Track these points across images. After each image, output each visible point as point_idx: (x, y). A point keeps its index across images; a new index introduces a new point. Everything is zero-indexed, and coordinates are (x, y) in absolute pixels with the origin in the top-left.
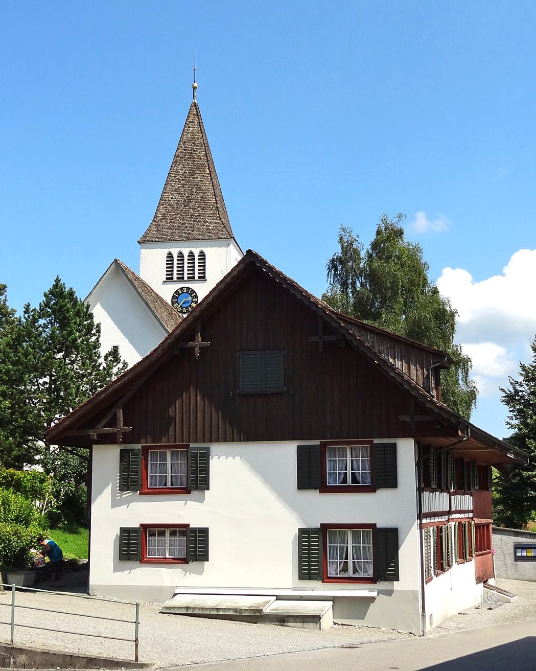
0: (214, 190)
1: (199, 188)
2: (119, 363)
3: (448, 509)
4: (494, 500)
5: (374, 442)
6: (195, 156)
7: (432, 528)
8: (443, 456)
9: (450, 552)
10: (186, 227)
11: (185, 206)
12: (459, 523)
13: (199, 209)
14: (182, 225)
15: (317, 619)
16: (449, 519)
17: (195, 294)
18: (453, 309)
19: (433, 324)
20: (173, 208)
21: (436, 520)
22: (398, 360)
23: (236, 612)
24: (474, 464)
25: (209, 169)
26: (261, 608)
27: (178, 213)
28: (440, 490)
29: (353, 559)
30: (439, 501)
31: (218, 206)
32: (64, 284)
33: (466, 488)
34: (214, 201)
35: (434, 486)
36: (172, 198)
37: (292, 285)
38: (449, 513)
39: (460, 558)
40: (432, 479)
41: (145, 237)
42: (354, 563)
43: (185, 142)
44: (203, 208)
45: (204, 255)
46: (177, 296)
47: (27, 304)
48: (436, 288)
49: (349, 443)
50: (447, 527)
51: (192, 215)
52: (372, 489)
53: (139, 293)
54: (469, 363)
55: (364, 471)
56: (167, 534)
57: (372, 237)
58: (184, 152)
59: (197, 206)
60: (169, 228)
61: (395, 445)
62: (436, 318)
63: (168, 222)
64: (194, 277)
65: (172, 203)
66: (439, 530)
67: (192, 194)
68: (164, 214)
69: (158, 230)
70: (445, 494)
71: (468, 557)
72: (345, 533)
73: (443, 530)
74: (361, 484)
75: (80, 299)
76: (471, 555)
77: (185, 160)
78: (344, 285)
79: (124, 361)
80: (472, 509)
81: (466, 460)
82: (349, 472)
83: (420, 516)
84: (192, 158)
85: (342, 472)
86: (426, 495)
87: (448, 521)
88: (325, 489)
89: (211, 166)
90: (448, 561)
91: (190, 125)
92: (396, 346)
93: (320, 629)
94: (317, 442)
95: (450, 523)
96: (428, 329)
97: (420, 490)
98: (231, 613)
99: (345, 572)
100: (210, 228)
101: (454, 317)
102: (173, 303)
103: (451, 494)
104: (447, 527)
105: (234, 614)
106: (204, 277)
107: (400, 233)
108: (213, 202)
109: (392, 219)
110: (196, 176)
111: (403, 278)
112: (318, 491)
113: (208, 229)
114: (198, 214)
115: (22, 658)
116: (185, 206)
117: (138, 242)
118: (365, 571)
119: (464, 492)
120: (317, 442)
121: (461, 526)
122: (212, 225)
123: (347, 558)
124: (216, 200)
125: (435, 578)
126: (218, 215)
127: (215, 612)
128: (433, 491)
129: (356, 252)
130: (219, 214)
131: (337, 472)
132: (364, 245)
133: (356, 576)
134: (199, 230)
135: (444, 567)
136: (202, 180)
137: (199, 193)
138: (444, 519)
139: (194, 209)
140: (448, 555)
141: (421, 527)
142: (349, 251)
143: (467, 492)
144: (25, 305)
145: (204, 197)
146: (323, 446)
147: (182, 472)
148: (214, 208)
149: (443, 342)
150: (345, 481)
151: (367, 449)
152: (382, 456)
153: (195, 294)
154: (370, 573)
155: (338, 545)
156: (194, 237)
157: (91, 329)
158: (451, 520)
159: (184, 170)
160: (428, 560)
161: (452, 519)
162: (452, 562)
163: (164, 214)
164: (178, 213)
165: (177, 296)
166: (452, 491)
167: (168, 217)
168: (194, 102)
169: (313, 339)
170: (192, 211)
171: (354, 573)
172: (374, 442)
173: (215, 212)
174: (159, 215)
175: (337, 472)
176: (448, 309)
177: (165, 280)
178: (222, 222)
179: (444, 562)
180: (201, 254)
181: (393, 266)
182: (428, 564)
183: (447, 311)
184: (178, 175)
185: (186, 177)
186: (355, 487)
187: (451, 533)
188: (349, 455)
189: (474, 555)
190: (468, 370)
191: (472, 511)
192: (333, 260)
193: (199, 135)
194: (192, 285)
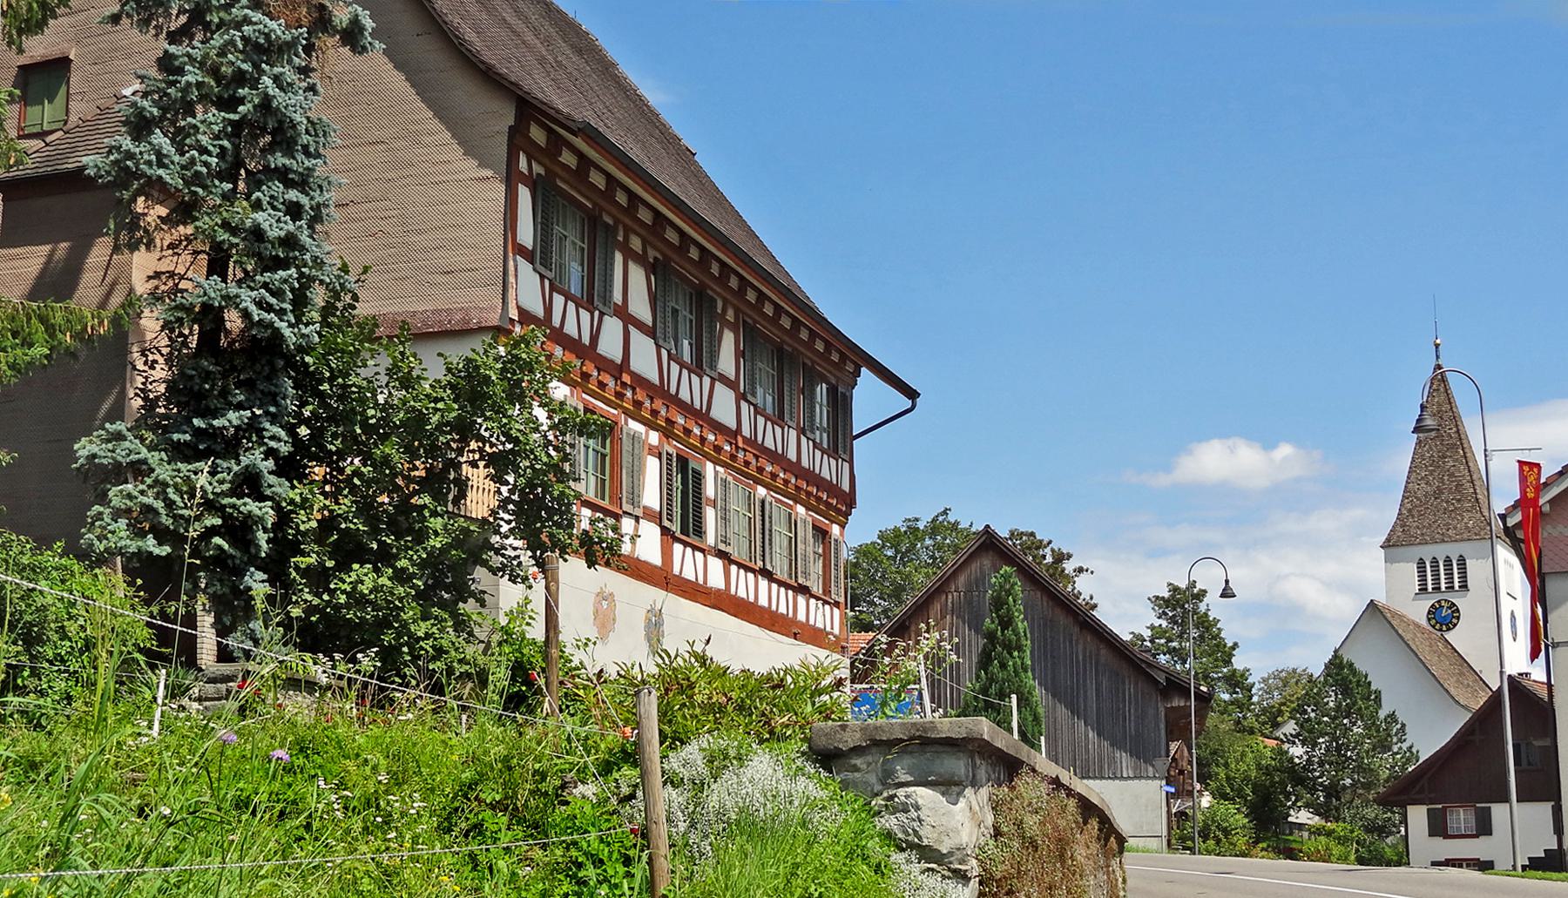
4: (1258, 829)
22: (970, 630)
25: (1463, 450)
31: (1479, 496)
34: (1472, 490)
41: (1388, 540)
44: (1459, 501)
60: (1418, 528)
68: (1410, 511)
88: (1447, 836)
89: (1465, 446)
106: (1466, 586)
113: (1467, 528)
134: (1455, 528)
137: (1453, 482)
139: (1447, 502)
156: (1450, 537)
163: (1410, 511)
167: (1415, 513)
193: (1446, 407)
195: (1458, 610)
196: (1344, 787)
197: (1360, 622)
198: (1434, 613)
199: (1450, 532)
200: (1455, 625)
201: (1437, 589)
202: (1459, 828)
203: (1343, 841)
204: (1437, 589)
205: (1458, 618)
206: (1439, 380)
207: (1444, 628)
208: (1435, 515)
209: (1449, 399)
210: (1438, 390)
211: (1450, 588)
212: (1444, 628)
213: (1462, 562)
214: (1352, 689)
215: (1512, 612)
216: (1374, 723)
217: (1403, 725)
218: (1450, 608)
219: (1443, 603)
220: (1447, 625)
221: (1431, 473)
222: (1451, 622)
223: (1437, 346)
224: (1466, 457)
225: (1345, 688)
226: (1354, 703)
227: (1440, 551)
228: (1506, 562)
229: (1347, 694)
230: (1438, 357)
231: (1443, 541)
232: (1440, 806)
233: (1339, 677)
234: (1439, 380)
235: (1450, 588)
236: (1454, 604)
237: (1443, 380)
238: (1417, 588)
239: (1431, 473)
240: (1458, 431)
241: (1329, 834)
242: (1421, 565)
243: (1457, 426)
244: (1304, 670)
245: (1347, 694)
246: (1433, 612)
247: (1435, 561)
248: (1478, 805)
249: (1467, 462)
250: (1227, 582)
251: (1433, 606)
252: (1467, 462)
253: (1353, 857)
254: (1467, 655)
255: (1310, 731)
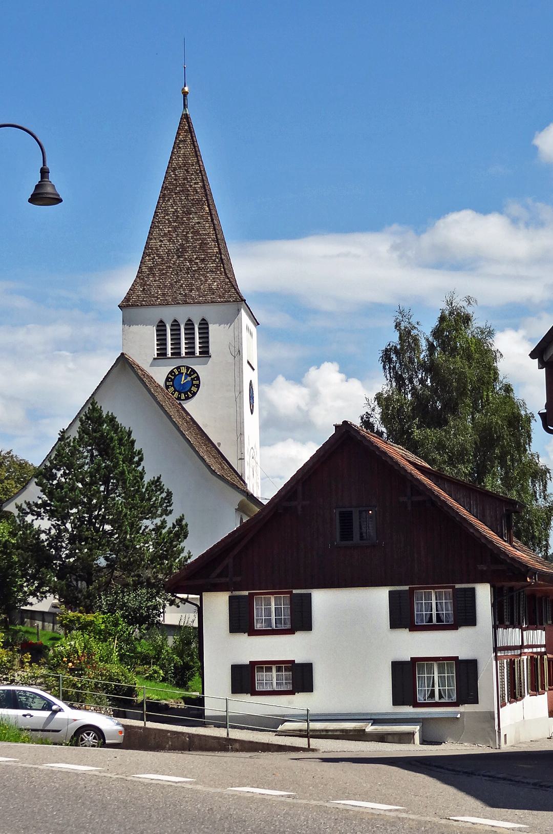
0: (216, 236)
1: (196, 233)
2: (162, 492)
3: (521, 644)
5: (456, 587)
6: (189, 188)
7: (505, 661)
8: (515, 598)
9: (523, 684)
10: (181, 286)
11: (179, 257)
12: (531, 657)
13: (197, 261)
14: (176, 282)
15: (412, 736)
16: (521, 653)
17: (196, 375)
18: (528, 412)
19: (506, 432)
20: (163, 259)
21: (510, 653)
23: (343, 732)
24: (546, 599)
25: (209, 206)
26: (364, 728)
27: (170, 267)
28: (513, 626)
29: (439, 687)
30: (512, 636)
32: (101, 407)
33: (538, 623)
34: (216, 250)
35: (507, 623)
36: (161, 246)
37: (493, 605)
38: (522, 647)
39: (532, 691)
40: (505, 617)
41: (127, 299)
42: (439, 690)
43: (175, 169)
45: (207, 324)
46: (173, 377)
47: (62, 430)
48: (509, 386)
49: (434, 588)
50: (520, 660)
51: (188, 269)
52: (454, 627)
53: (158, 403)
54: (548, 474)
55: (448, 610)
56: (274, 670)
57: (435, 323)
58: (175, 182)
59: (195, 257)
61: (473, 590)
62: (510, 424)
63: (157, 279)
64: (194, 352)
65: (162, 253)
66: (511, 664)
67: (188, 242)
68: (151, 269)
69: (144, 289)
70: (517, 629)
71: (540, 690)
72: (432, 665)
73: (516, 662)
74: (445, 623)
75: (121, 424)
76: (543, 688)
77: (176, 193)
78: (399, 379)
79: (168, 490)
80: (544, 643)
81: (538, 595)
82: (434, 612)
83: (496, 649)
84: (185, 191)
85: (429, 613)
86: (500, 630)
87: (520, 655)
90: (521, 692)
91: (181, 146)
92: (471, 494)
93: (414, 743)
94: (406, 588)
95: (522, 657)
96: (500, 438)
97: (495, 628)
98: (338, 733)
99: (432, 698)
100: (213, 287)
101: (530, 422)
102: (167, 387)
103: (523, 630)
104: (520, 660)
105: (341, 734)
106: (207, 352)
107: (467, 319)
108: (215, 251)
109: (459, 302)
110: (191, 216)
111: (472, 373)
112: (246, 634)
113: (210, 289)
114: (196, 268)
115: (237, 746)
116: (179, 257)
117: (119, 306)
118: (450, 697)
119: (536, 627)
120: (406, 588)
121: (533, 661)
122: (216, 284)
123: (433, 686)
124: (220, 250)
125: (508, 704)
126: (222, 270)
127: (324, 733)
128: (506, 627)
129: (416, 340)
130: (224, 268)
131: (424, 613)
132: (425, 329)
133: (442, 701)
134: (198, 289)
135: (517, 696)
136: (200, 221)
137: (197, 240)
138: (518, 652)
139: (191, 261)
140: (521, 687)
141: (496, 658)
142: (407, 336)
143: (539, 627)
144: (60, 431)
145: (203, 244)
146: (411, 591)
147: (286, 616)
148: (217, 260)
149: (519, 451)
150: (431, 620)
151: (449, 594)
152: (463, 599)
153: (196, 375)
154: (454, 698)
155: (426, 675)
156: (193, 299)
157: (133, 457)
158: (523, 654)
159: (175, 208)
160: (503, 688)
161: (525, 653)
162: (524, 693)
163: (151, 269)
164: (170, 267)
165: (173, 377)
166: (524, 626)
168: (184, 113)
169: (401, 499)
170: (188, 264)
171: (440, 699)
172: (456, 587)
173: (219, 265)
174: (145, 269)
175: (424, 613)
176: (523, 413)
177: (156, 356)
178: (228, 278)
179: (517, 691)
180: (203, 322)
181: (458, 363)
182: (502, 691)
183: (522, 416)
184: (168, 215)
185: (178, 217)
186: (441, 625)
187: (524, 666)
188: (434, 597)
189: (547, 689)
190: (546, 483)
191: (544, 646)
192: (387, 350)
194: (189, 362)
195: (198, 378)
196: (100, 569)
197: (113, 371)
198: (172, 380)
199: (193, 293)
200: (194, 394)
201: (176, 354)
202: (269, 622)
203: (103, 636)
204: (176, 354)
205: (198, 386)
206: (186, 125)
207: (183, 397)
208: (177, 274)
209: (196, 151)
210: (185, 141)
211: (191, 354)
212: (183, 397)
213: (204, 326)
214: (113, 449)
215: (251, 381)
216: (138, 491)
217: (169, 494)
218: (190, 375)
219: (184, 370)
220: (186, 393)
221: (175, 230)
222: (190, 391)
223: (185, 94)
224: (211, 215)
225: (104, 446)
226: (116, 465)
227: (182, 313)
228: (247, 328)
229: (107, 454)
230: (185, 106)
231: (186, 303)
232: (246, 593)
233: (98, 435)
234: (186, 125)
235: (191, 354)
236: (194, 371)
237: (190, 131)
238: (156, 352)
239: (175, 229)
240: (204, 187)
241: (84, 627)
242: (161, 328)
243: (203, 181)
244: (8, 453)
245: (107, 454)
246: (172, 378)
247: (176, 325)
248: (295, 591)
249: (212, 220)
250: (44, 172)
251: (172, 372)
252: (212, 220)
253: (115, 656)
254: (206, 426)
255: (61, 500)
